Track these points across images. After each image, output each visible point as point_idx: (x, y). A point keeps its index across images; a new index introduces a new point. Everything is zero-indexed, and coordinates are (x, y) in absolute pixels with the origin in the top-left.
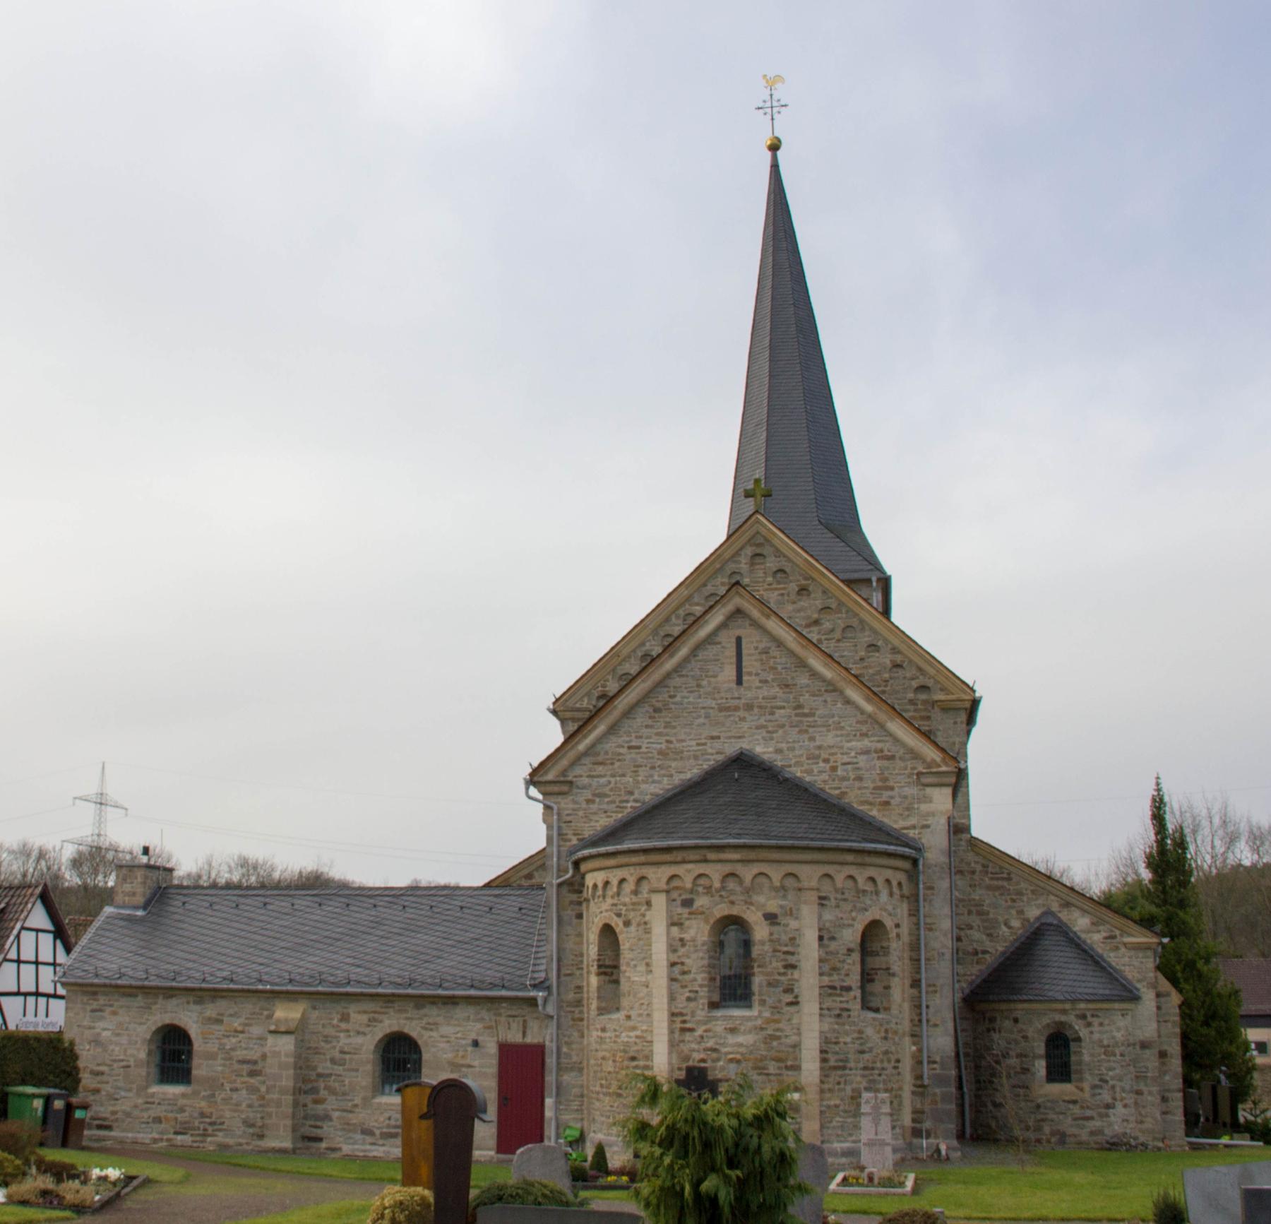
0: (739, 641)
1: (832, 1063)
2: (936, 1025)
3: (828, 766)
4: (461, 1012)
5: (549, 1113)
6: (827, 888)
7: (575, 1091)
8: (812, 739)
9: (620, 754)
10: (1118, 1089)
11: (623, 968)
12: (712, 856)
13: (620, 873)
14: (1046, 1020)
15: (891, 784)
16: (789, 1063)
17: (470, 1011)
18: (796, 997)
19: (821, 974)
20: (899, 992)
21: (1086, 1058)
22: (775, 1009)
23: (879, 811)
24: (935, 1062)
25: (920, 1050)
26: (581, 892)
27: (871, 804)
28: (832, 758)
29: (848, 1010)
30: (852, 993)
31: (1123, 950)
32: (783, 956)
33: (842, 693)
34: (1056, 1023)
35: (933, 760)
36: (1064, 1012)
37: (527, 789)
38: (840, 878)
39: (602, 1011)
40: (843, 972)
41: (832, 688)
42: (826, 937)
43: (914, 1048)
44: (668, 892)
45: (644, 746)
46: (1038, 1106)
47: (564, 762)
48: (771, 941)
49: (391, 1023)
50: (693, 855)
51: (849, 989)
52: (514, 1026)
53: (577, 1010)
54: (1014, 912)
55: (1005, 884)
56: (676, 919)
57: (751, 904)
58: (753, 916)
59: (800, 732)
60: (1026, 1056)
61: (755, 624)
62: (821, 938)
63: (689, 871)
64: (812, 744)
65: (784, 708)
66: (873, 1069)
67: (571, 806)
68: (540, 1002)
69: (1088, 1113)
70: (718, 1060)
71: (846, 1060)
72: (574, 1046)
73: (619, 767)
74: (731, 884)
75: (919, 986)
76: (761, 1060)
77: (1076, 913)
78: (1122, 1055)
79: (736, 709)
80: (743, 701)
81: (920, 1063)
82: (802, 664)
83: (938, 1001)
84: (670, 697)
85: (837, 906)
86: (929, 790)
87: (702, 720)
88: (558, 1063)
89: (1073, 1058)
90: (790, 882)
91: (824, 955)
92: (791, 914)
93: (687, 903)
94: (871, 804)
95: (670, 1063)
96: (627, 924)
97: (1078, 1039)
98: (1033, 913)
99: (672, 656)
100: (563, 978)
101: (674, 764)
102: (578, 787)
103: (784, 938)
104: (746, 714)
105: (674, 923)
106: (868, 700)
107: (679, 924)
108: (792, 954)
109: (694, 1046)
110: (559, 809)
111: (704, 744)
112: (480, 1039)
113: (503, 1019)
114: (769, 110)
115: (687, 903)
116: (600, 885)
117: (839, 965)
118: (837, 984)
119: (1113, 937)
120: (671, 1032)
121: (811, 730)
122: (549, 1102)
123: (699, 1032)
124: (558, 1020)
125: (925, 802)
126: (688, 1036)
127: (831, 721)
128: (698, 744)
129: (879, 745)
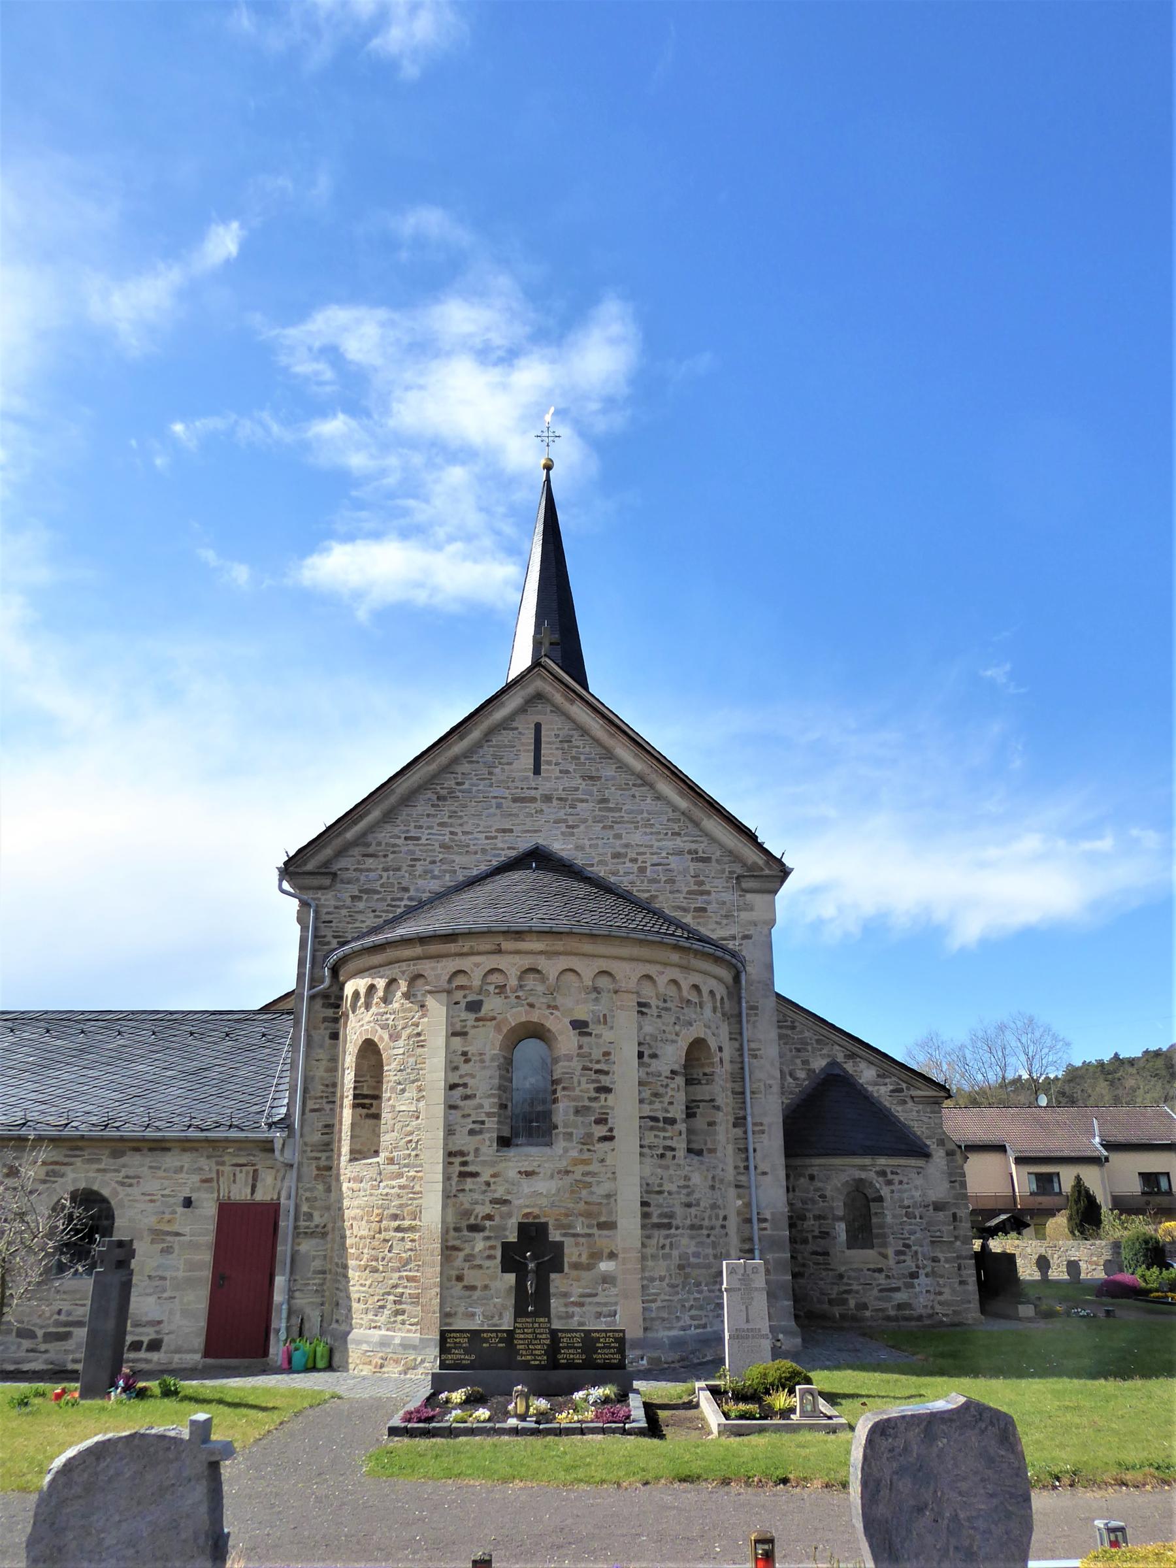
0: (538, 727)
1: (655, 1220)
2: (764, 1173)
3: (636, 866)
4: (170, 1160)
5: (279, 1297)
6: (648, 993)
7: (317, 1264)
8: (618, 836)
9: (394, 845)
10: (920, 1256)
11: (385, 1095)
12: (507, 945)
13: (393, 971)
14: (844, 1177)
15: (707, 887)
16: (603, 1219)
17: (186, 1160)
18: (611, 1130)
19: (641, 1101)
20: (724, 1135)
21: (889, 1219)
22: (587, 1140)
23: (694, 918)
24: (765, 1220)
25: (748, 1205)
26: (338, 1006)
27: (685, 910)
28: (640, 858)
29: (673, 1149)
30: (676, 1127)
31: (910, 1104)
32: (594, 1077)
33: (651, 786)
34: (854, 1180)
35: (755, 863)
36: (863, 1168)
37: (281, 881)
38: (662, 981)
39: (356, 1155)
40: (667, 1099)
41: (644, 781)
42: (646, 1054)
43: (740, 1202)
44: (449, 992)
45: (424, 837)
46: (841, 1276)
47: (328, 852)
48: (578, 1055)
49: (79, 1176)
50: (486, 945)
51: (672, 1121)
52: (241, 1177)
53: (324, 1155)
54: (798, 1061)
55: (789, 1032)
56: (458, 1028)
57: (556, 1008)
58: (559, 1025)
59: (604, 828)
60: (824, 1218)
61: (558, 710)
62: (641, 1055)
63: (477, 965)
64: (618, 842)
65: (587, 801)
66: (701, 1227)
67: (333, 903)
68: (278, 1145)
69: (895, 1283)
70: (510, 1215)
71: (671, 1216)
72: (318, 1204)
73: (392, 860)
74: (531, 982)
75: (745, 1125)
76: (567, 1215)
77: (863, 1065)
78: (921, 1218)
79: (533, 800)
80: (540, 792)
81: (749, 1221)
82: (609, 755)
83: (766, 1142)
84: (458, 784)
85: (659, 1016)
86: (749, 896)
87: (492, 810)
88: (296, 1227)
89: (874, 1220)
90: (603, 982)
91: (644, 1076)
92: (605, 1023)
93: (474, 1007)
94: (685, 910)
95: (443, 1222)
96: (395, 1037)
97: (880, 1199)
98: (819, 1063)
99: (461, 738)
100: (308, 1115)
101: (457, 859)
102: (342, 882)
103: (597, 1054)
104: (544, 807)
105: (456, 1033)
106: (682, 795)
107: (462, 1034)
108: (607, 1073)
109: (476, 1196)
110: (317, 906)
111: (496, 838)
112: (194, 1197)
113: (227, 1169)
114: (546, 434)
115: (474, 1007)
116: (362, 991)
117: (662, 1090)
118: (660, 1115)
119: (901, 1090)
120: (447, 1178)
121: (616, 826)
122: (280, 1281)
123: (485, 1177)
124: (299, 1169)
125: (745, 910)
126: (469, 1183)
127: (639, 817)
128: (487, 838)
129: (694, 846)
